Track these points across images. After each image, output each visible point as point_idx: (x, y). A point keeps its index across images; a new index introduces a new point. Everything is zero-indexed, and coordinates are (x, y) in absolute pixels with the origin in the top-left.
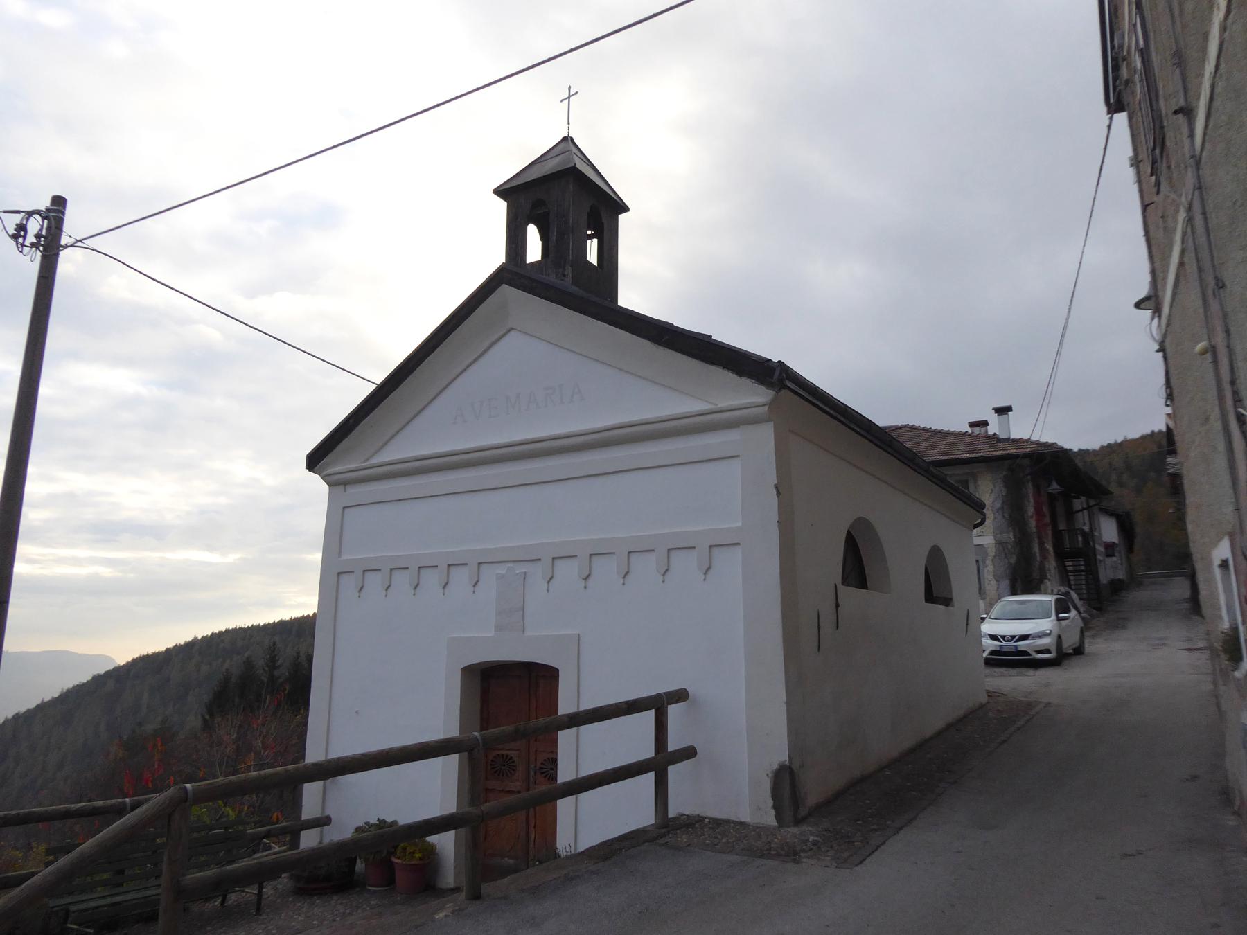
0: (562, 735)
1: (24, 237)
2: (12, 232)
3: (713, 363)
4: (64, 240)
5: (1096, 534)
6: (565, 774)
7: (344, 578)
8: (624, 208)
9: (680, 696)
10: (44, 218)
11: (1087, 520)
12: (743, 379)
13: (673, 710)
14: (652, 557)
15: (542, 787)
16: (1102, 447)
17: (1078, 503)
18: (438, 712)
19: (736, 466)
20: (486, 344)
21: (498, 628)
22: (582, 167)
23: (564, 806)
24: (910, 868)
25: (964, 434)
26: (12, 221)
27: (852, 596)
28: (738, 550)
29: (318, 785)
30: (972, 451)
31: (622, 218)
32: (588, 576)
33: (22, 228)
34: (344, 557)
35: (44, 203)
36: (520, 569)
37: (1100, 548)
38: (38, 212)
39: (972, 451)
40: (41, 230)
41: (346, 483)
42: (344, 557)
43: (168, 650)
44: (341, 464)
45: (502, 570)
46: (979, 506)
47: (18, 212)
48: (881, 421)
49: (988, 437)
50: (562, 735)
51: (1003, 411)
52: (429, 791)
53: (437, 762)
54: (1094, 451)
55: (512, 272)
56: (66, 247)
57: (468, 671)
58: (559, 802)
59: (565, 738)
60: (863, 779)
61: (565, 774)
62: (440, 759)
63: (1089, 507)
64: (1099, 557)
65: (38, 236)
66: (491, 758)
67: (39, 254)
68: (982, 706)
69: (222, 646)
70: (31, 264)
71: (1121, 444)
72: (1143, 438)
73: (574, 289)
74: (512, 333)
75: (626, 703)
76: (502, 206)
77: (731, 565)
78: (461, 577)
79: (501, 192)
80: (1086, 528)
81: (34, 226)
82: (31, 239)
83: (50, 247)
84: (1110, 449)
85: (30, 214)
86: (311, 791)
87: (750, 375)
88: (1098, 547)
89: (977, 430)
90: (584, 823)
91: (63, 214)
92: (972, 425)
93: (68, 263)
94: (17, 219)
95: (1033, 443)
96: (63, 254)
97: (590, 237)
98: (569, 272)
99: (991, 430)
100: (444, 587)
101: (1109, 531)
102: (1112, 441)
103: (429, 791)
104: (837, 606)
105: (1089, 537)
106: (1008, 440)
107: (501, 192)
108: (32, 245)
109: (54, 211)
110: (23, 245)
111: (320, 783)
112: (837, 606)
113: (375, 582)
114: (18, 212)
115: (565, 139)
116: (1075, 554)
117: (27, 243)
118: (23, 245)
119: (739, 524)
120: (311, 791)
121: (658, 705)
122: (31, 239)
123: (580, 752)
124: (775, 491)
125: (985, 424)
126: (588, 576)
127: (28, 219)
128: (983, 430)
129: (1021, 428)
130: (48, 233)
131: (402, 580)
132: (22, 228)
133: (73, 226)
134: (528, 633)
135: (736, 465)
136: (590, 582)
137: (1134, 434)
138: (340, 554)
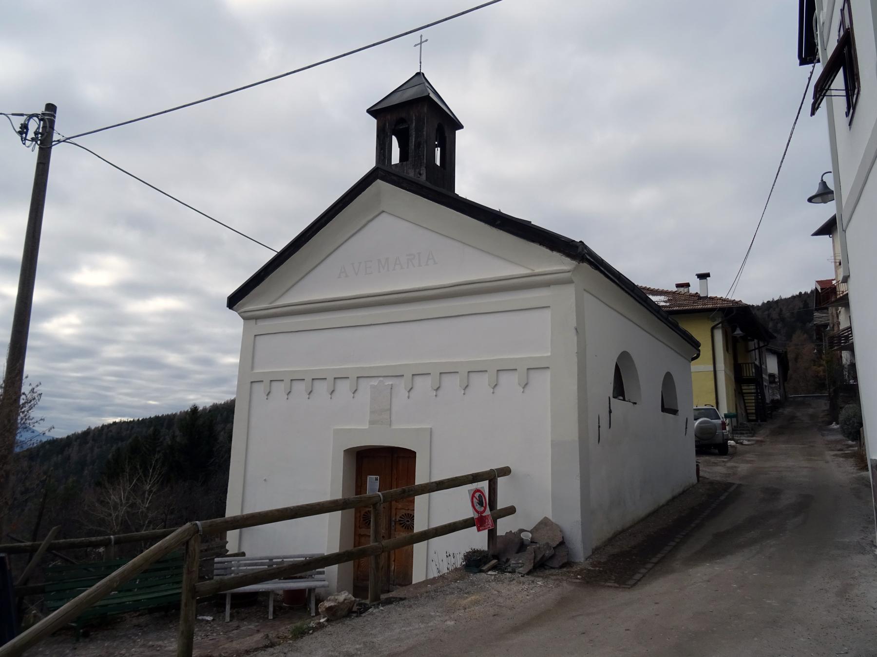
0: (418, 499)
1: (26, 134)
2: (18, 129)
3: (533, 241)
4: (56, 137)
5: (763, 367)
6: (419, 526)
7: (255, 385)
8: (460, 127)
9: (505, 471)
10: (40, 120)
11: (757, 357)
12: (555, 253)
13: (501, 481)
14: (486, 376)
15: (402, 535)
16: (763, 304)
17: (752, 344)
18: (328, 481)
19: (547, 314)
20: (364, 222)
21: (372, 422)
22: (432, 95)
23: (419, 548)
24: (690, 589)
25: (674, 293)
26: (18, 121)
27: (617, 403)
28: (548, 373)
29: (236, 532)
30: (679, 306)
31: (458, 133)
32: (438, 388)
33: (24, 128)
34: (256, 371)
35: (41, 109)
36: (389, 382)
37: (765, 377)
38: (36, 115)
39: (679, 306)
40: (38, 128)
41: (257, 318)
42: (256, 371)
43: (68, 437)
44: (251, 304)
45: (375, 382)
46: (696, 345)
47: (22, 115)
48: (639, 281)
49: (692, 295)
50: (418, 499)
51: (703, 276)
52: (323, 535)
53: (325, 518)
54: (758, 306)
55: (382, 171)
56: (59, 141)
57: (348, 452)
58: (415, 545)
59: (420, 501)
60: (623, 531)
61: (419, 526)
62: (328, 514)
63: (759, 348)
64: (765, 384)
65: (36, 133)
66: (363, 513)
67: (37, 147)
68: (693, 486)
69: (110, 434)
70: (30, 155)
71: (777, 301)
72: (793, 297)
73: (428, 184)
74: (384, 215)
75: (472, 475)
76: (372, 123)
77: (543, 382)
78: (344, 387)
79: (372, 112)
80: (757, 363)
81: (33, 125)
82: (31, 135)
83: (45, 143)
84: (769, 306)
85: (31, 116)
86: (232, 536)
87: (559, 251)
88: (764, 376)
89: (681, 290)
90: (431, 560)
91: (55, 117)
92: (678, 286)
93: (57, 152)
94: (22, 120)
95: (724, 300)
96: (54, 150)
97: (437, 146)
98: (423, 171)
99: (693, 290)
100: (310, 393)
101: (772, 365)
102: (771, 300)
103: (323, 535)
104: (610, 412)
105: (760, 370)
106: (707, 297)
107: (372, 112)
108: (33, 140)
109: (48, 115)
110: (26, 139)
111: (238, 530)
112: (610, 412)
113: (279, 389)
114: (22, 115)
115: (418, 74)
116: (749, 381)
117: (29, 137)
118: (26, 139)
119: (549, 354)
120: (232, 536)
121: (492, 477)
122: (31, 135)
123: (429, 511)
124: (574, 331)
125: (687, 285)
126: (438, 388)
127: (29, 120)
128: (686, 290)
129: (718, 289)
130: (43, 131)
131: (300, 388)
132: (24, 128)
133: (61, 129)
134: (394, 427)
135: (547, 313)
136: (440, 392)
137: (787, 294)
138: (252, 368)
